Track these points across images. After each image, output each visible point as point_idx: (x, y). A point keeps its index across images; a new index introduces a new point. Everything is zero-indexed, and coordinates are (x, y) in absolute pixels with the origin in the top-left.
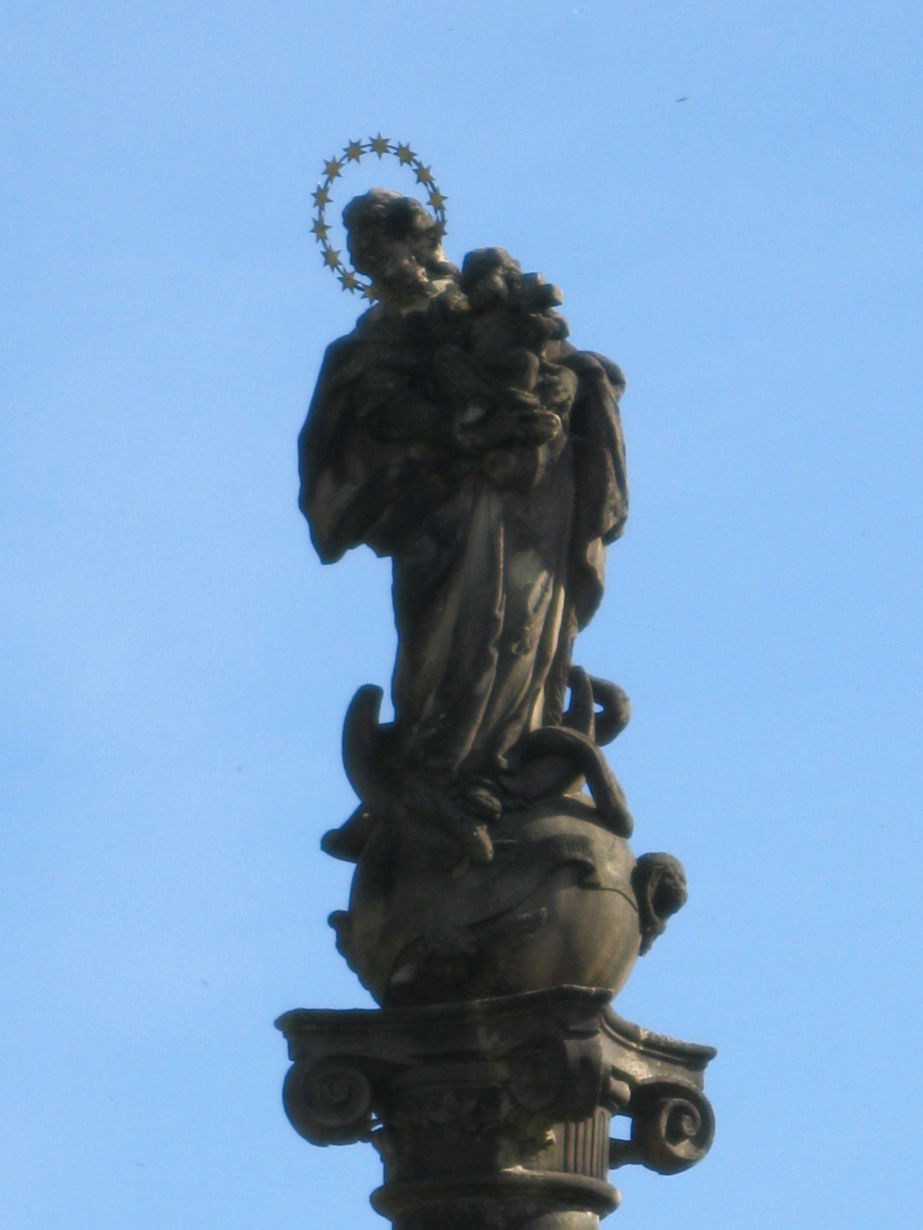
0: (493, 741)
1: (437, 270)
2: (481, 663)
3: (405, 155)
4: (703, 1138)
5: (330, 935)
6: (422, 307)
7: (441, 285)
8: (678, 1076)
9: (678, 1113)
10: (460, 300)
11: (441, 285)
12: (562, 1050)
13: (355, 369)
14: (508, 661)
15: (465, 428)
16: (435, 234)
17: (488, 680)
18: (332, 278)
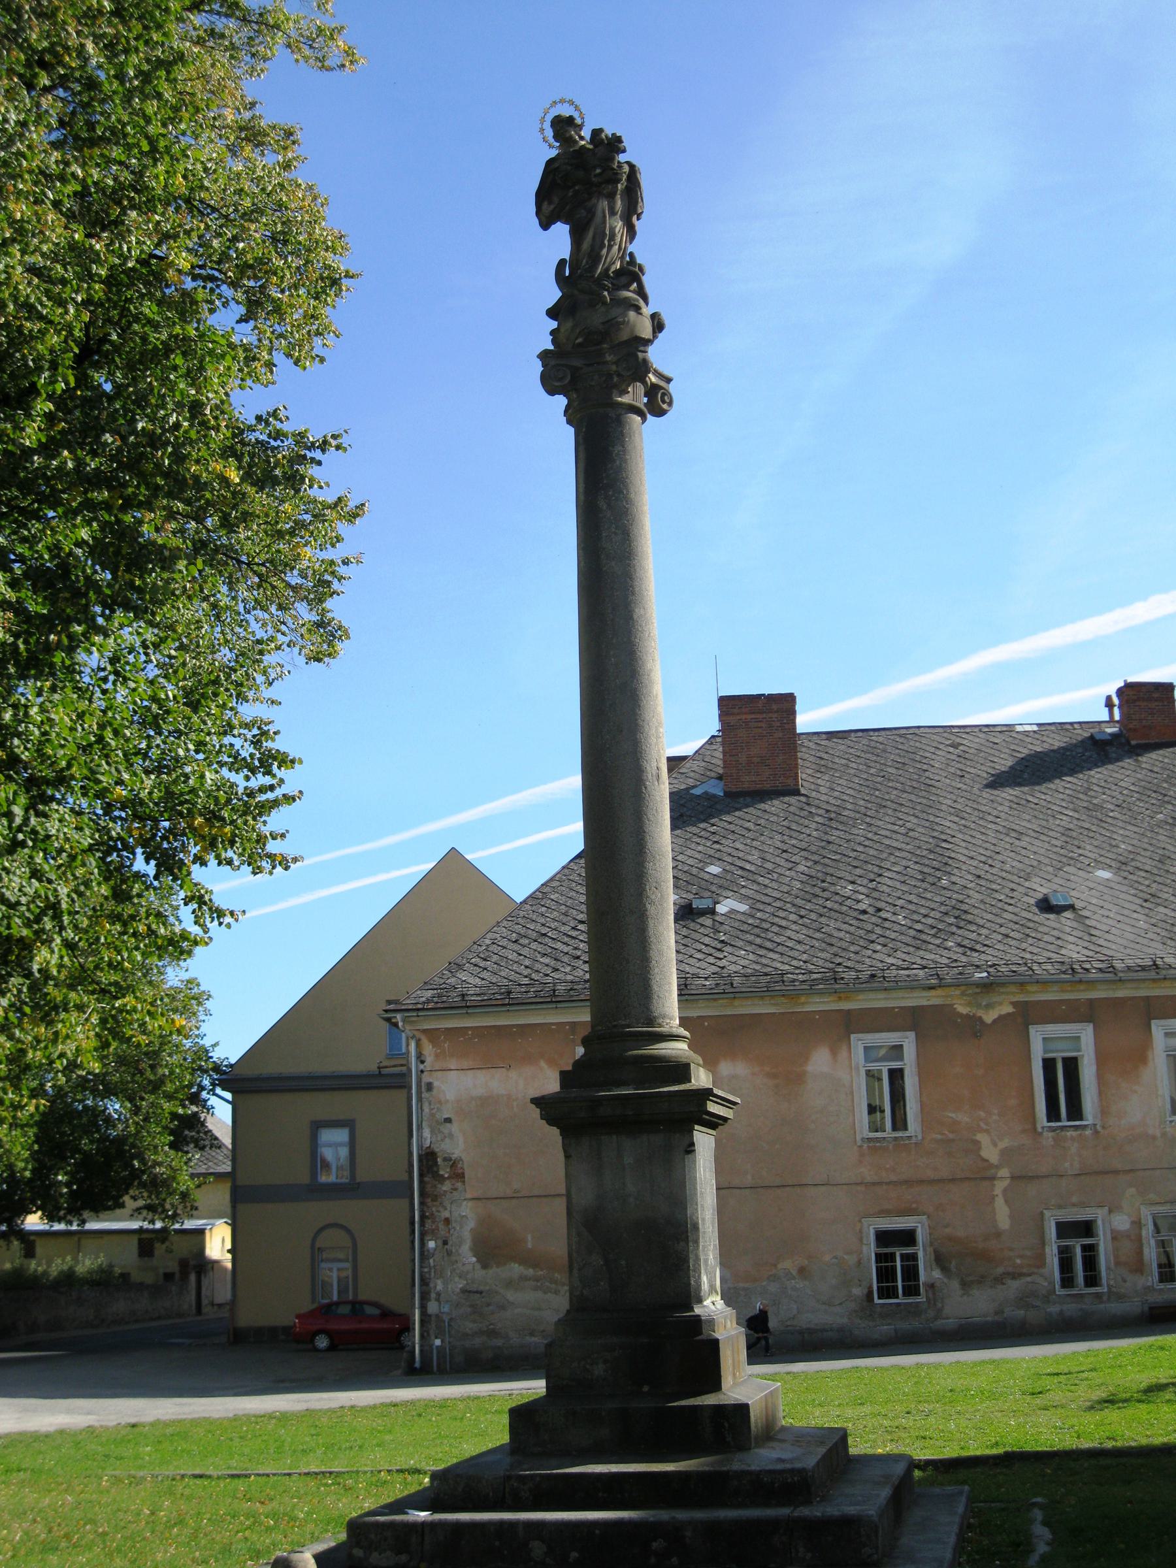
0: (608, 269)
1: (582, 138)
2: (602, 246)
3: (571, 103)
4: (670, 404)
5: (538, 367)
6: (577, 148)
7: (583, 143)
8: (662, 384)
9: (664, 395)
10: (591, 147)
11: (583, 143)
12: (637, 356)
13: (556, 165)
14: (610, 247)
15: (596, 176)
16: (580, 127)
17: (604, 251)
18: (546, 146)
